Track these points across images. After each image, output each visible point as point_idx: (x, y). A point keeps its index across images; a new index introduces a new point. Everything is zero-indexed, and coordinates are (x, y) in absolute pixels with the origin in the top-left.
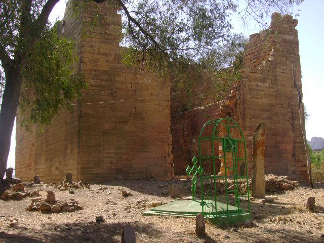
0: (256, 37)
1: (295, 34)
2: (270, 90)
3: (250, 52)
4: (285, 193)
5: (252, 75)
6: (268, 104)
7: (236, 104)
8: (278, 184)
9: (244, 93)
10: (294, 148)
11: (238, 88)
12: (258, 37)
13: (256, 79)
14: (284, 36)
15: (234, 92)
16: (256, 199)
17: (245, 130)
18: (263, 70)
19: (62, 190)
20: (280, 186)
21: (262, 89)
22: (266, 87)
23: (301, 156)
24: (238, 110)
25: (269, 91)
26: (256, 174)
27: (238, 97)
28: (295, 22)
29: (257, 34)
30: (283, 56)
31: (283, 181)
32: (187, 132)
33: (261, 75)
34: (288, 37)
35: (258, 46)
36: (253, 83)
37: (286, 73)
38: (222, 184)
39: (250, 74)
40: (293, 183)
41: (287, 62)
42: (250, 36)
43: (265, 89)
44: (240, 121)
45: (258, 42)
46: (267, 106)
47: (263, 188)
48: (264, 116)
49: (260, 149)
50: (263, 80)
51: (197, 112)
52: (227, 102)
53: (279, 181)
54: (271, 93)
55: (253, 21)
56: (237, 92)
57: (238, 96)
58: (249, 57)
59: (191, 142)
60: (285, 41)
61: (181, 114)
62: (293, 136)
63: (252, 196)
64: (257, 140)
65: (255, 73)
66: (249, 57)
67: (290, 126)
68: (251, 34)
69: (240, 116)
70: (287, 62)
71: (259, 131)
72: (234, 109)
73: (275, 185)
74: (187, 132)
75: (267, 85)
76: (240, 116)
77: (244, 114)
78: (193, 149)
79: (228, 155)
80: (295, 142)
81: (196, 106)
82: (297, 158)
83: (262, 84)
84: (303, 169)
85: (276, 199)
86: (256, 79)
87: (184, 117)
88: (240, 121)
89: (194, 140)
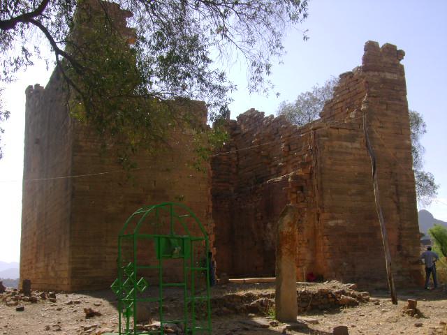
0: (348, 77)
1: (401, 71)
2: (361, 152)
3: (341, 99)
4: (339, 312)
5: (334, 132)
6: (359, 174)
7: (311, 174)
8: (333, 297)
9: (321, 158)
10: (400, 237)
11: (314, 151)
12: (351, 77)
13: (339, 138)
14: (382, 75)
15: (309, 156)
16: (280, 324)
17: (323, 212)
18: (351, 124)
19: (8, 305)
20: (336, 300)
21: (350, 151)
22: (356, 148)
23: (411, 248)
24: (315, 183)
25: (360, 155)
26: (281, 285)
27: (314, 163)
28: (401, 54)
29: (350, 73)
30: (382, 103)
31: (343, 292)
32: (260, 214)
33: (347, 132)
34: (389, 76)
35: (351, 89)
36: (336, 143)
37: (387, 128)
38: (242, 298)
39: (331, 130)
40: (360, 295)
41: (389, 112)
42: (341, 76)
43: (354, 151)
44: (317, 198)
45: (352, 84)
46: (356, 177)
47: (294, 305)
48: (354, 191)
49: (287, 246)
50: (352, 139)
51: (272, 185)
52: (300, 172)
53: (337, 293)
54: (363, 157)
55: (235, 51)
56: (312, 157)
57: (314, 163)
58: (340, 105)
59: (265, 228)
60: (384, 81)
61: (252, 187)
62: (398, 219)
63: (276, 318)
64: (282, 233)
65: (338, 129)
66: (340, 105)
67: (393, 206)
68: (342, 73)
69: (316, 191)
70: (389, 112)
71: (285, 218)
72: (308, 181)
73: (328, 298)
74: (260, 214)
75: (357, 145)
76: (316, 191)
77: (322, 189)
78: (268, 238)
79: (299, 248)
80: (401, 229)
81: (272, 176)
82: (405, 252)
83: (349, 144)
84: (415, 268)
85: (316, 322)
86: (339, 138)
87: (257, 192)
88: (317, 198)
89: (269, 226)
